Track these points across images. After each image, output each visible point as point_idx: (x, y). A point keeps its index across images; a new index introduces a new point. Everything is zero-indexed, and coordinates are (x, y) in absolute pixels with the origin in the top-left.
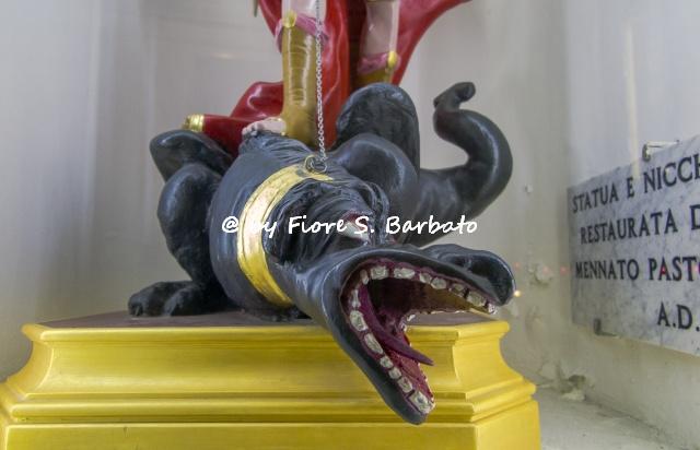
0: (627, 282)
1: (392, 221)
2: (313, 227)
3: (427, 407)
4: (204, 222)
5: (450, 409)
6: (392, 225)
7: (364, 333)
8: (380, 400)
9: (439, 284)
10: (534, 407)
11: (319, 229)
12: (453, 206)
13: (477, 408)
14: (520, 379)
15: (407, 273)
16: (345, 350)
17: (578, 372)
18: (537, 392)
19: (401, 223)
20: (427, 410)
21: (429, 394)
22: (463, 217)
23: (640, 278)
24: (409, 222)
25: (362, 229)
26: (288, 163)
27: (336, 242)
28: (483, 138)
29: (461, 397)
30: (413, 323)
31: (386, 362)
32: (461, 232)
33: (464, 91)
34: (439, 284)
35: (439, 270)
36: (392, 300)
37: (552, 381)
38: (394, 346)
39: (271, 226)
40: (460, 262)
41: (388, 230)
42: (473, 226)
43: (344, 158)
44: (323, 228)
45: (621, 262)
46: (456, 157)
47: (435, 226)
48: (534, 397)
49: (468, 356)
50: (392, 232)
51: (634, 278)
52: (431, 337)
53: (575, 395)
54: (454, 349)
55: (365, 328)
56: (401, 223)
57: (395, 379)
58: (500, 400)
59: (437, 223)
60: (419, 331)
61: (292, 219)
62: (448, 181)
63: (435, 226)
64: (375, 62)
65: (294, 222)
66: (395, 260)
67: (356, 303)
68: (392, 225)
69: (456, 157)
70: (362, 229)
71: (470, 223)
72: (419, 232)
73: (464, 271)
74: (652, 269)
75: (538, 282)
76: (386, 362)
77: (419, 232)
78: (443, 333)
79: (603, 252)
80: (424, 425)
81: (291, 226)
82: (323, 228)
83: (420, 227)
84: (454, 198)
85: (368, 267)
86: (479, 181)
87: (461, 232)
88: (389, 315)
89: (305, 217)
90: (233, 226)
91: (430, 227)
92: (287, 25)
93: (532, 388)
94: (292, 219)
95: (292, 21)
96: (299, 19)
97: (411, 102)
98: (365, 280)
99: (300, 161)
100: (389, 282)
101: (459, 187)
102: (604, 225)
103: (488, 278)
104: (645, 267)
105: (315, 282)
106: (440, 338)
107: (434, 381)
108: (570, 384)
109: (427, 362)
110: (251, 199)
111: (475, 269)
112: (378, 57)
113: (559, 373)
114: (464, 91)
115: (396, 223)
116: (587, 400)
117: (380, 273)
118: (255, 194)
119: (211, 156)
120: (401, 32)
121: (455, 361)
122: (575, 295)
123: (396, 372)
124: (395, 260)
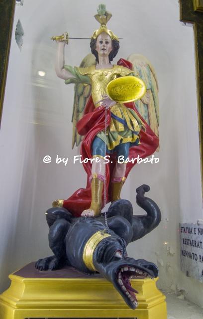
0: (194, 260)
1: (121, 158)
2: (85, 160)
3: (137, 304)
4: (82, 259)
5: (142, 305)
6: (121, 159)
7: (122, 285)
8: (124, 302)
10: (165, 303)
11: (87, 161)
12: (142, 229)
13: (149, 304)
14: (161, 294)
16: (115, 286)
17: (183, 289)
18: (166, 299)
19: (125, 159)
20: (137, 306)
21: (137, 301)
23: (198, 261)
24: (128, 158)
26: (98, 230)
27: (114, 258)
29: (144, 301)
33: (146, 188)
37: (174, 291)
38: (127, 285)
40: (146, 266)
41: (119, 162)
45: (193, 254)
46: (143, 213)
47: (59, 160)
48: (166, 300)
49: (147, 289)
50: (120, 163)
51: (196, 260)
52: (137, 283)
53: (181, 297)
54: (143, 286)
55: (122, 284)
56: (125, 159)
57: (129, 296)
58: (155, 302)
60: (133, 281)
61: (75, 157)
63: (59, 160)
64: (118, 180)
65: (76, 158)
67: (120, 277)
69: (143, 213)
73: (147, 269)
74: (200, 258)
75: (170, 254)
76: (127, 293)
78: (140, 282)
79: (189, 249)
80: (136, 309)
81: (75, 160)
83: (133, 160)
84: (142, 227)
85: (123, 267)
86: (151, 220)
88: (126, 277)
90: (48, 160)
91: (138, 161)
92: (94, 178)
93: (165, 297)
94: (75, 157)
95: (95, 176)
96: (98, 176)
97: (131, 205)
98: (122, 271)
99: (102, 229)
101: (144, 224)
102: (189, 240)
104: (199, 258)
106: (139, 283)
107: (138, 296)
108: (180, 293)
109: (137, 292)
110: (88, 242)
111: (149, 268)
112: (119, 179)
113: (177, 288)
114: (146, 188)
115: (122, 159)
116: (185, 299)
117: (126, 269)
118: (90, 240)
119: (71, 211)
120: (127, 167)
121: (143, 289)
122: (181, 261)
123: (130, 296)
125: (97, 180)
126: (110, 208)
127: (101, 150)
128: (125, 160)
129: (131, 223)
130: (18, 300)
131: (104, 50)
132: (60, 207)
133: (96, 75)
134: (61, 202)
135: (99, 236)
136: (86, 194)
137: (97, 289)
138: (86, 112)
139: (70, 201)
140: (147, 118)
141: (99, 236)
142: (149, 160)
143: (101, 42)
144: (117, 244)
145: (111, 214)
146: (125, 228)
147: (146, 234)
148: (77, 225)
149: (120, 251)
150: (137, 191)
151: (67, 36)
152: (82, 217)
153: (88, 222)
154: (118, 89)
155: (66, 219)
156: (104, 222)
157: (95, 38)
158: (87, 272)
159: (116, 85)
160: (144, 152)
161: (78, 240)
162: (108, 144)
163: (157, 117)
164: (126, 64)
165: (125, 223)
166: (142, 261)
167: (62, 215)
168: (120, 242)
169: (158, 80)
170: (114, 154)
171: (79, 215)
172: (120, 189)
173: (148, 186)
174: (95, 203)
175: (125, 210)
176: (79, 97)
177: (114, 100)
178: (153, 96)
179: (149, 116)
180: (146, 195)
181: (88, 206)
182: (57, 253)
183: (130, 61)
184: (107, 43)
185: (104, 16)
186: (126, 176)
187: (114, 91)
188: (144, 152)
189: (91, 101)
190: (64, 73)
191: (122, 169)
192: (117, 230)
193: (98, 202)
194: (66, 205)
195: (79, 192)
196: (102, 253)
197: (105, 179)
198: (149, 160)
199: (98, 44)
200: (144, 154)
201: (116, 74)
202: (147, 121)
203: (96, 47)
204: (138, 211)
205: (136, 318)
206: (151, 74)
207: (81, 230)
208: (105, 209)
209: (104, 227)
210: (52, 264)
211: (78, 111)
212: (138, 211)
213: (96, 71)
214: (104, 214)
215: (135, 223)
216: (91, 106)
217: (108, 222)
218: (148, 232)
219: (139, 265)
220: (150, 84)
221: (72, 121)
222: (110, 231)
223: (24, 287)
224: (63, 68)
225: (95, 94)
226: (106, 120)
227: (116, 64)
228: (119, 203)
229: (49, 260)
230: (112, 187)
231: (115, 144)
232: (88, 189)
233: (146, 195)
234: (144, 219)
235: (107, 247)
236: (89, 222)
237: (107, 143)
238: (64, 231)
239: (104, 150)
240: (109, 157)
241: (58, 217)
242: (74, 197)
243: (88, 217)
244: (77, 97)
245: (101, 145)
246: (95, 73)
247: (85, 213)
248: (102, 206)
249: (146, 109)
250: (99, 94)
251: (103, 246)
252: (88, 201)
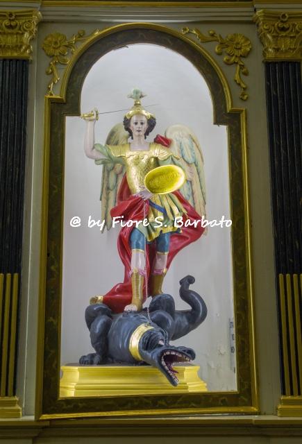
2: (128, 223)
9: (180, 356)
11: (132, 224)
12: (186, 326)
15: (174, 353)
25: (159, 224)
26: (142, 323)
28: (196, 302)
30: (175, 365)
31: (169, 372)
32: (222, 227)
33: (190, 280)
34: (180, 356)
35: (180, 353)
36: (170, 359)
39: (101, 223)
40: (185, 351)
43: (154, 317)
44: (134, 224)
46: (188, 307)
47: (92, 223)
54: (185, 373)
60: (175, 366)
61: (114, 218)
62: (184, 317)
63: (92, 223)
65: (116, 220)
66: (172, 350)
69: (188, 307)
70: (159, 224)
72: (195, 226)
73: (186, 353)
75: (221, 354)
76: (169, 372)
77: (195, 226)
82: (134, 224)
84: (187, 323)
87: (222, 227)
89: (123, 217)
91: (202, 223)
99: (146, 322)
100: (170, 355)
101: (189, 319)
103: (190, 354)
105: (153, 355)
114: (190, 280)
115: (181, 221)
117: (168, 353)
124: (172, 350)
125: (137, 275)
126: (152, 303)
127: (140, 243)
129: (174, 319)
130: (75, 384)
131: (139, 131)
132: (99, 303)
133: (131, 158)
134: (100, 298)
135: (142, 329)
136: (126, 289)
137: (143, 375)
138: (121, 197)
139: (108, 297)
140: (191, 197)
141: (142, 329)
142: (217, 223)
143: (136, 123)
144: (160, 334)
145: (153, 308)
146: (167, 322)
147: (190, 331)
148: (120, 320)
149: (162, 340)
150: (181, 283)
151: (97, 112)
152: (126, 312)
153: (132, 316)
154: (156, 181)
155: (108, 316)
156: (147, 316)
157: (128, 118)
158: (135, 362)
159: (154, 177)
160: (187, 238)
161: (124, 332)
162: (148, 236)
163: (203, 194)
164: (163, 142)
165: (167, 317)
166: (181, 347)
167: (103, 311)
168: (162, 333)
169: (202, 152)
170: (153, 249)
171: (121, 310)
172: (161, 282)
173: (87, 309)
174: (137, 296)
175: (168, 304)
176: (109, 172)
177: (152, 192)
178: (197, 169)
179: (193, 194)
180: (191, 287)
181: (129, 302)
182: (100, 349)
183: (168, 137)
184: (142, 124)
185: (139, 96)
186: (168, 267)
187: (152, 184)
188: (187, 238)
189: (125, 183)
190: (95, 153)
191: (163, 261)
192: (160, 322)
193: (140, 298)
194: (105, 301)
195: (118, 287)
196: (147, 341)
197: (146, 273)
198: (218, 222)
199: (132, 124)
200: (187, 241)
201: (153, 157)
202: (190, 202)
203: (130, 126)
204: (181, 305)
206: (194, 145)
207: (126, 324)
208: (147, 304)
209: (147, 320)
210: (97, 359)
211: (108, 188)
212: (181, 305)
213: (130, 153)
214: (146, 309)
215: (178, 318)
216: (125, 189)
217: (151, 316)
218: (192, 329)
219: (179, 350)
220: (193, 157)
221: (101, 200)
222: (152, 323)
223: (78, 373)
224: (94, 148)
225: (130, 179)
226: (144, 209)
227: (153, 141)
228: (160, 298)
229: (92, 356)
230: (153, 280)
231: (155, 235)
233: (191, 287)
234: (189, 314)
235: (151, 336)
236: (132, 316)
237: (146, 235)
238: (107, 326)
239: (143, 243)
241: (100, 313)
242: (112, 293)
243: (131, 312)
244: (106, 172)
245: (139, 239)
246: (130, 155)
247: (127, 308)
248: (143, 300)
249: (189, 186)
250: (137, 184)
251: (148, 336)
252: (127, 296)
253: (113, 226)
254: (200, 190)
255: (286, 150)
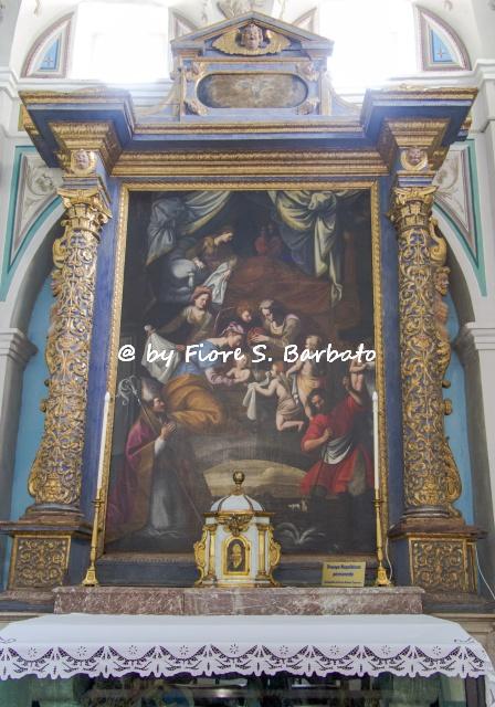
2: (210, 355)
6: (290, 353)
22: (330, 345)
42: (371, 355)
47: (333, 356)
59: (334, 351)
61: (189, 348)
63: (333, 356)
65: (191, 350)
68: (290, 353)
70: (261, 357)
71: (369, 352)
77: (318, 361)
90: (129, 354)
91: (329, 356)
94: (189, 348)
115: (294, 352)
128: (300, 354)
198: (353, 354)
205: (476, 686)
232: (110, 122)
240: (265, 347)
253: (187, 360)
254: (243, 72)
255: (218, 160)
